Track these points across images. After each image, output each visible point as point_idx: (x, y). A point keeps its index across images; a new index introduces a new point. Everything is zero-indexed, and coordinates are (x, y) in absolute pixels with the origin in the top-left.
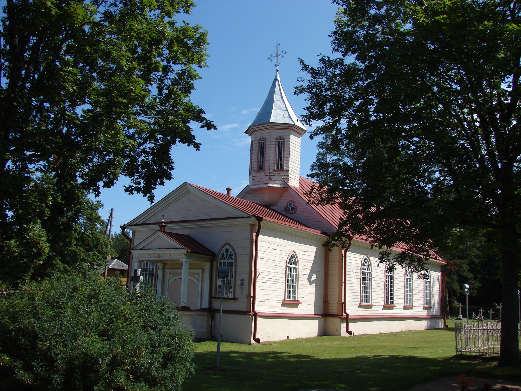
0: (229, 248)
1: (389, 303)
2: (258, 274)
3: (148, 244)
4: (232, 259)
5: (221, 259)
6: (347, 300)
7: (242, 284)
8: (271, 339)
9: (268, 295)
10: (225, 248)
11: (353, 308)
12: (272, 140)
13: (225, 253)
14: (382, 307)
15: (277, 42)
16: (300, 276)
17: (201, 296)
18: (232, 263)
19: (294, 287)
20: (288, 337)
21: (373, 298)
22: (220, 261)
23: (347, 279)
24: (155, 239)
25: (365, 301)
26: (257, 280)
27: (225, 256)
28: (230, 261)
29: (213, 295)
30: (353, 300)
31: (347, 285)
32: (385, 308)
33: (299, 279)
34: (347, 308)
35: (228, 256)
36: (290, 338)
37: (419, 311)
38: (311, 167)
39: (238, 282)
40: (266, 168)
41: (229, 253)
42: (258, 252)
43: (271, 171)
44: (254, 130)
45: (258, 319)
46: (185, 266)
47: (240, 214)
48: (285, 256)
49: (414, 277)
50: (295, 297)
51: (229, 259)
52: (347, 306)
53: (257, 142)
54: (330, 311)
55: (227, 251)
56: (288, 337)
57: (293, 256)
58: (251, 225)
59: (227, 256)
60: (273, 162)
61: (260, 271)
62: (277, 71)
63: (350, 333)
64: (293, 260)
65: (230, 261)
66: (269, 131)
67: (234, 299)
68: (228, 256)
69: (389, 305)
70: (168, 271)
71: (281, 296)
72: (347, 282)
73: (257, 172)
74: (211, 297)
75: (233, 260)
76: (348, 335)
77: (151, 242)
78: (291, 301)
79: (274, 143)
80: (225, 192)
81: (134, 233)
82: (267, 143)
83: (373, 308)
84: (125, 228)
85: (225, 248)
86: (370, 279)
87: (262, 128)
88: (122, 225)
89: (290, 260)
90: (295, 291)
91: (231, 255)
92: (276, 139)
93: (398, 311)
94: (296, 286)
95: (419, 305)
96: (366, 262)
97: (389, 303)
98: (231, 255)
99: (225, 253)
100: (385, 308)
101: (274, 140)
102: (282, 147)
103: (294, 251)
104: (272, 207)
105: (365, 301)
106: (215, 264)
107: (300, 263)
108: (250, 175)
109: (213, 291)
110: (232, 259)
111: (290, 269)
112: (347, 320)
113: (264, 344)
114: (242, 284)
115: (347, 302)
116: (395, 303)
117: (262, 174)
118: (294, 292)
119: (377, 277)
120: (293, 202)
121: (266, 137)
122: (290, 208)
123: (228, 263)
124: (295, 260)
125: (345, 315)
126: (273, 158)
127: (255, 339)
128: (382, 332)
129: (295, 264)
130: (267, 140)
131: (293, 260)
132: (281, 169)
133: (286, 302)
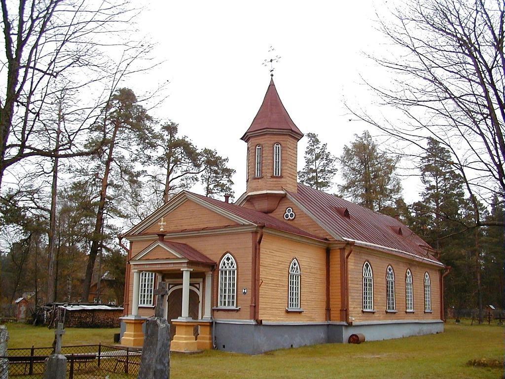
10: (226, 256)
27: (226, 265)
41: (230, 261)
59: (228, 264)
99: (226, 262)
122: (289, 214)
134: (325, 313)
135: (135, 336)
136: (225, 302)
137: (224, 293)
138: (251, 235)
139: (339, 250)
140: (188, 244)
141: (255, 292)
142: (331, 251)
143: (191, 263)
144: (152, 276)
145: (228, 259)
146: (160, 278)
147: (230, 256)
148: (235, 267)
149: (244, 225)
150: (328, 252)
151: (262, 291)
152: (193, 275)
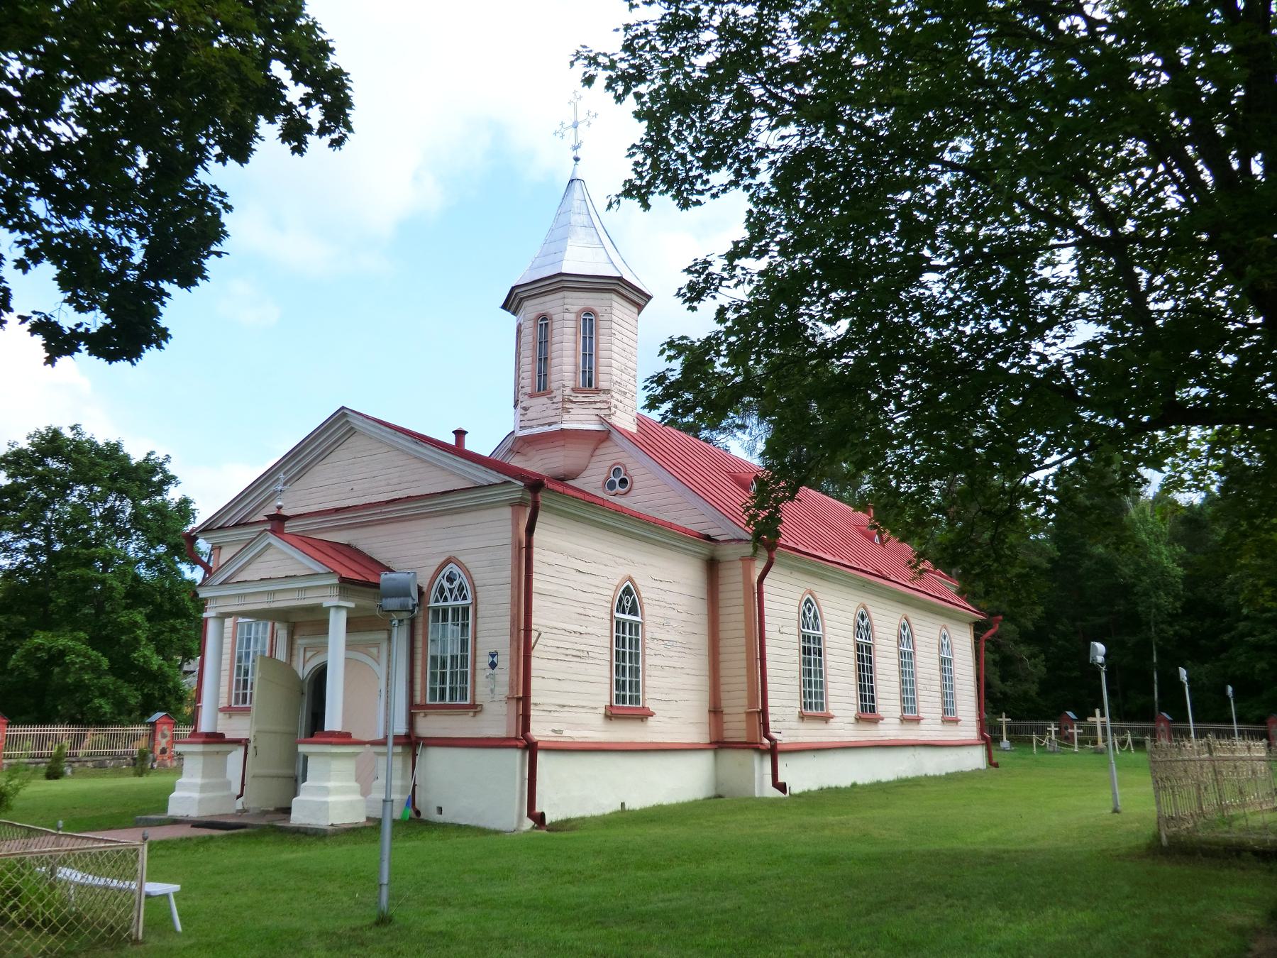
0: (456, 570)
1: (868, 710)
2: (534, 634)
4: (465, 598)
5: (437, 601)
6: (770, 702)
7: (493, 665)
8: (575, 813)
9: (569, 693)
10: (446, 571)
11: (785, 720)
12: (567, 316)
13: (446, 585)
14: (853, 720)
16: (649, 643)
17: (387, 703)
18: (465, 610)
19: (635, 672)
20: (623, 804)
21: (830, 699)
22: (432, 604)
23: (768, 650)
25: (813, 703)
26: (534, 653)
27: (447, 593)
28: (460, 602)
29: (418, 700)
30: (784, 702)
31: (768, 664)
32: (611, 715)
33: (647, 651)
34: (771, 725)
35: (455, 592)
36: (627, 807)
37: (968, 728)
38: (687, 279)
39: (483, 662)
40: (554, 386)
41: (456, 583)
42: (535, 576)
43: (568, 392)
44: (522, 295)
45: (541, 757)
46: (338, 623)
48: (608, 592)
49: (917, 648)
50: (637, 697)
51: (456, 599)
52: (771, 718)
53: (530, 323)
54: (739, 731)
56: (623, 804)
57: (627, 591)
59: (451, 591)
60: (571, 368)
61: (541, 629)
62: (577, 159)
63: (782, 787)
64: (628, 600)
68: (455, 592)
69: (869, 715)
71: (602, 694)
72: (768, 657)
73: (531, 396)
76: (778, 793)
78: (626, 703)
79: (572, 324)
80: (451, 440)
82: (555, 325)
83: (881, 726)
85: (446, 571)
86: (820, 651)
89: (620, 600)
90: (637, 683)
91: (461, 588)
92: (578, 314)
93: (890, 729)
94: (637, 669)
95: (933, 716)
96: (809, 610)
97: (868, 710)
99: (446, 585)
100: (611, 715)
101: (572, 316)
102: (591, 333)
103: (630, 579)
104: (571, 483)
105: (813, 703)
107: (647, 610)
108: (515, 406)
109: (418, 687)
110: (465, 598)
111: (620, 625)
112: (774, 752)
113: (559, 826)
114: (493, 665)
115: (770, 710)
116: (880, 710)
117: (544, 400)
118: (635, 686)
119: (836, 645)
120: (624, 466)
121: (551, 311)
122: (617, 481)
123: (455, 610)
124: (634, 601)
125: (766, 741)
126: (572, 360)
128: (860, 782)
129: (633, 611)
130: (555, 318)
131: (628, 600)
132: (590, 385)
133: (614, 711)
134: (1138, 847)
135: (203, 788)
136: (443, 691)
137: (462, 667)
138: (507, 512)
139: (740, 564)
140: (353, 543)
141: (913, 746)
142: (721, 566)
143: (347, 586)
144: (265, 632)
145: (451, 579)
146: (282, 634)
147: (456, 570)
148: (470, 597)
149: (491, 485)
150: (712, 567)
151: (478, 640)
152: (353, 625)
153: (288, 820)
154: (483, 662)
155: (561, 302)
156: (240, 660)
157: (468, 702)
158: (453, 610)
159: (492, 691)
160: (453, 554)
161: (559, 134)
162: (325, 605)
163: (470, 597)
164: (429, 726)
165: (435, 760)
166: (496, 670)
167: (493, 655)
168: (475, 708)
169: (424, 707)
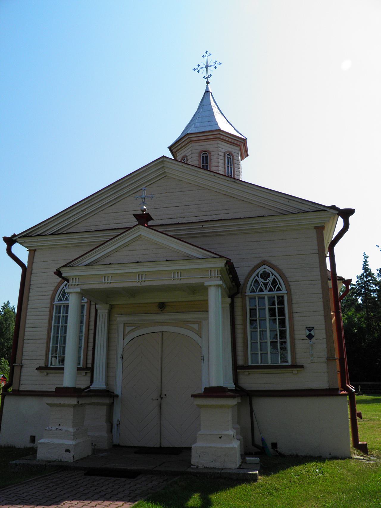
0: (269, 270)
3: (107, 256)
4: (279, 289)
5: (253, 291)
7: (310, 337)
15: (207, 54)
24: (126, 245)
28: (275, 293)
29: (240, 362)
35: (270, 285)
39: (301, 334)
41: (271, 279)
47: (264, 213)
51: (271, 290)
55: (265, 276)
58: (316, 228)
59: (266, 285)
65: (275, 293)
66: (216, 142)
67: (297, 366)
70: (120, 320)
74: (236, 368)
75: (284, 291)
77: (116, 250)
81: (32, 252)
84: (14, 242)
85: (261, 270)
87: (212, 137)
88: (9, 235)
91: (274, 282)
98: (274, 282)
99: (261, 280)
106: (238, 301)
110: (279, 289)
127: (356, 445)
130: (212, 153)
148: (284, 288)
153: (35, 457)
154: (301, 334)
155: (216, 145)
156: (283, 334)
157: (290, 363)
158: (64, 306)
159: (312, 355)
160: (265, 259)
161: (198, 69)
162: (206, 284)
163: (284, 288)
164: (252, 381)
165: (266, 408)
166: (313, 340)
167: (310, 330)
168: (297, 366)
169: (246, 367)
